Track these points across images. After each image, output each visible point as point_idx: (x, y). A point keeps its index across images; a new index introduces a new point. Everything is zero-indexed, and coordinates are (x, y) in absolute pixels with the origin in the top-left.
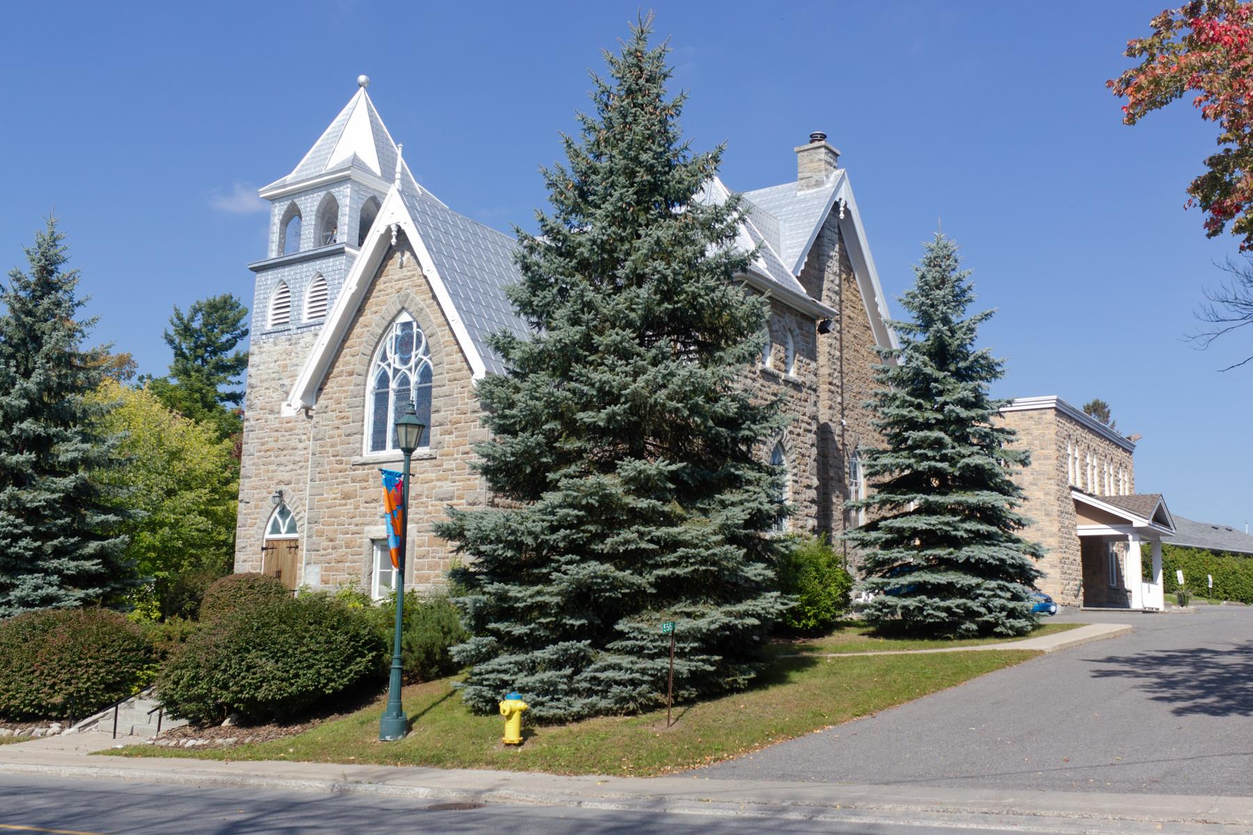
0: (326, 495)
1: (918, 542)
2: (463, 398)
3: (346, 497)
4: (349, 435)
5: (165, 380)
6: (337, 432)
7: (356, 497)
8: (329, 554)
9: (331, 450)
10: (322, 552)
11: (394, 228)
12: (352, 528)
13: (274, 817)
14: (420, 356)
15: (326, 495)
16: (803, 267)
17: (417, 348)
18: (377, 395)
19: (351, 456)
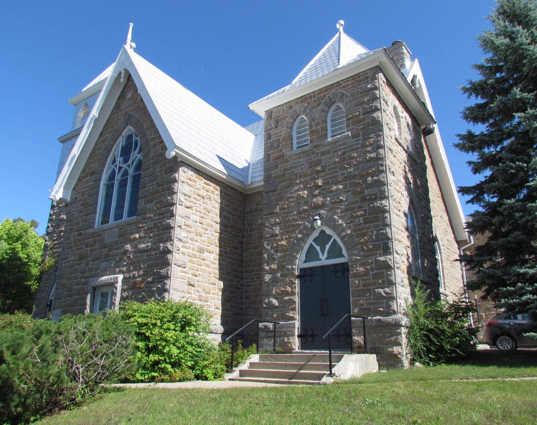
0: (69, 259)
1: (517, 297)
2: (161, 175)
3: (81, 258)
4: (87, 215)
5: (485, 82)
6: (80, 215)
7: (87, 258)
8: (68, 300)
9: (76, 227)
10: (63, 300)
11: (123, 72)
12: (83, 280)
13: (392, 100)
14: (136, 155)
15: (69, 259)
16: (392, 251)
17: (135, 150)
18: (107, 186)
19: (87, 229)
